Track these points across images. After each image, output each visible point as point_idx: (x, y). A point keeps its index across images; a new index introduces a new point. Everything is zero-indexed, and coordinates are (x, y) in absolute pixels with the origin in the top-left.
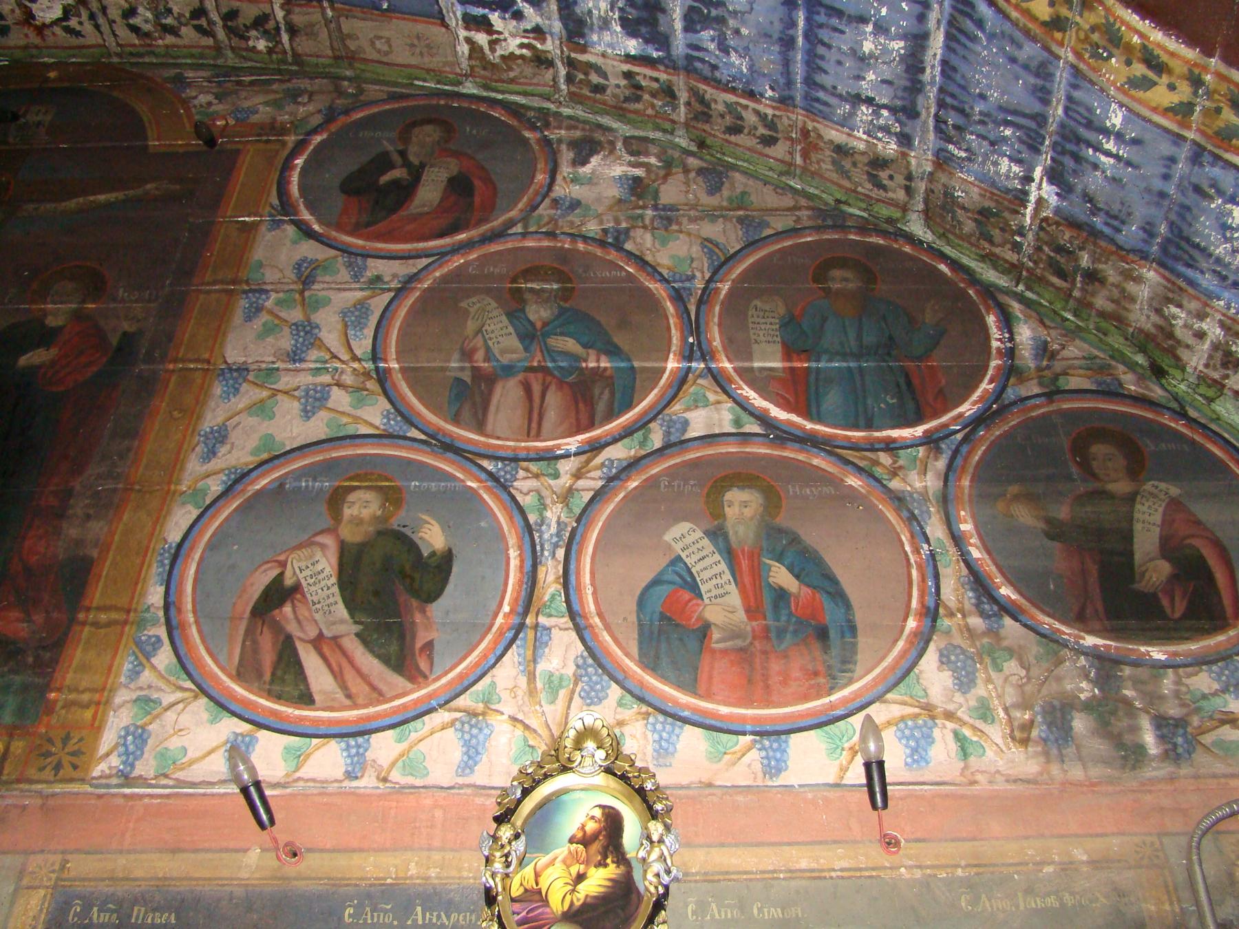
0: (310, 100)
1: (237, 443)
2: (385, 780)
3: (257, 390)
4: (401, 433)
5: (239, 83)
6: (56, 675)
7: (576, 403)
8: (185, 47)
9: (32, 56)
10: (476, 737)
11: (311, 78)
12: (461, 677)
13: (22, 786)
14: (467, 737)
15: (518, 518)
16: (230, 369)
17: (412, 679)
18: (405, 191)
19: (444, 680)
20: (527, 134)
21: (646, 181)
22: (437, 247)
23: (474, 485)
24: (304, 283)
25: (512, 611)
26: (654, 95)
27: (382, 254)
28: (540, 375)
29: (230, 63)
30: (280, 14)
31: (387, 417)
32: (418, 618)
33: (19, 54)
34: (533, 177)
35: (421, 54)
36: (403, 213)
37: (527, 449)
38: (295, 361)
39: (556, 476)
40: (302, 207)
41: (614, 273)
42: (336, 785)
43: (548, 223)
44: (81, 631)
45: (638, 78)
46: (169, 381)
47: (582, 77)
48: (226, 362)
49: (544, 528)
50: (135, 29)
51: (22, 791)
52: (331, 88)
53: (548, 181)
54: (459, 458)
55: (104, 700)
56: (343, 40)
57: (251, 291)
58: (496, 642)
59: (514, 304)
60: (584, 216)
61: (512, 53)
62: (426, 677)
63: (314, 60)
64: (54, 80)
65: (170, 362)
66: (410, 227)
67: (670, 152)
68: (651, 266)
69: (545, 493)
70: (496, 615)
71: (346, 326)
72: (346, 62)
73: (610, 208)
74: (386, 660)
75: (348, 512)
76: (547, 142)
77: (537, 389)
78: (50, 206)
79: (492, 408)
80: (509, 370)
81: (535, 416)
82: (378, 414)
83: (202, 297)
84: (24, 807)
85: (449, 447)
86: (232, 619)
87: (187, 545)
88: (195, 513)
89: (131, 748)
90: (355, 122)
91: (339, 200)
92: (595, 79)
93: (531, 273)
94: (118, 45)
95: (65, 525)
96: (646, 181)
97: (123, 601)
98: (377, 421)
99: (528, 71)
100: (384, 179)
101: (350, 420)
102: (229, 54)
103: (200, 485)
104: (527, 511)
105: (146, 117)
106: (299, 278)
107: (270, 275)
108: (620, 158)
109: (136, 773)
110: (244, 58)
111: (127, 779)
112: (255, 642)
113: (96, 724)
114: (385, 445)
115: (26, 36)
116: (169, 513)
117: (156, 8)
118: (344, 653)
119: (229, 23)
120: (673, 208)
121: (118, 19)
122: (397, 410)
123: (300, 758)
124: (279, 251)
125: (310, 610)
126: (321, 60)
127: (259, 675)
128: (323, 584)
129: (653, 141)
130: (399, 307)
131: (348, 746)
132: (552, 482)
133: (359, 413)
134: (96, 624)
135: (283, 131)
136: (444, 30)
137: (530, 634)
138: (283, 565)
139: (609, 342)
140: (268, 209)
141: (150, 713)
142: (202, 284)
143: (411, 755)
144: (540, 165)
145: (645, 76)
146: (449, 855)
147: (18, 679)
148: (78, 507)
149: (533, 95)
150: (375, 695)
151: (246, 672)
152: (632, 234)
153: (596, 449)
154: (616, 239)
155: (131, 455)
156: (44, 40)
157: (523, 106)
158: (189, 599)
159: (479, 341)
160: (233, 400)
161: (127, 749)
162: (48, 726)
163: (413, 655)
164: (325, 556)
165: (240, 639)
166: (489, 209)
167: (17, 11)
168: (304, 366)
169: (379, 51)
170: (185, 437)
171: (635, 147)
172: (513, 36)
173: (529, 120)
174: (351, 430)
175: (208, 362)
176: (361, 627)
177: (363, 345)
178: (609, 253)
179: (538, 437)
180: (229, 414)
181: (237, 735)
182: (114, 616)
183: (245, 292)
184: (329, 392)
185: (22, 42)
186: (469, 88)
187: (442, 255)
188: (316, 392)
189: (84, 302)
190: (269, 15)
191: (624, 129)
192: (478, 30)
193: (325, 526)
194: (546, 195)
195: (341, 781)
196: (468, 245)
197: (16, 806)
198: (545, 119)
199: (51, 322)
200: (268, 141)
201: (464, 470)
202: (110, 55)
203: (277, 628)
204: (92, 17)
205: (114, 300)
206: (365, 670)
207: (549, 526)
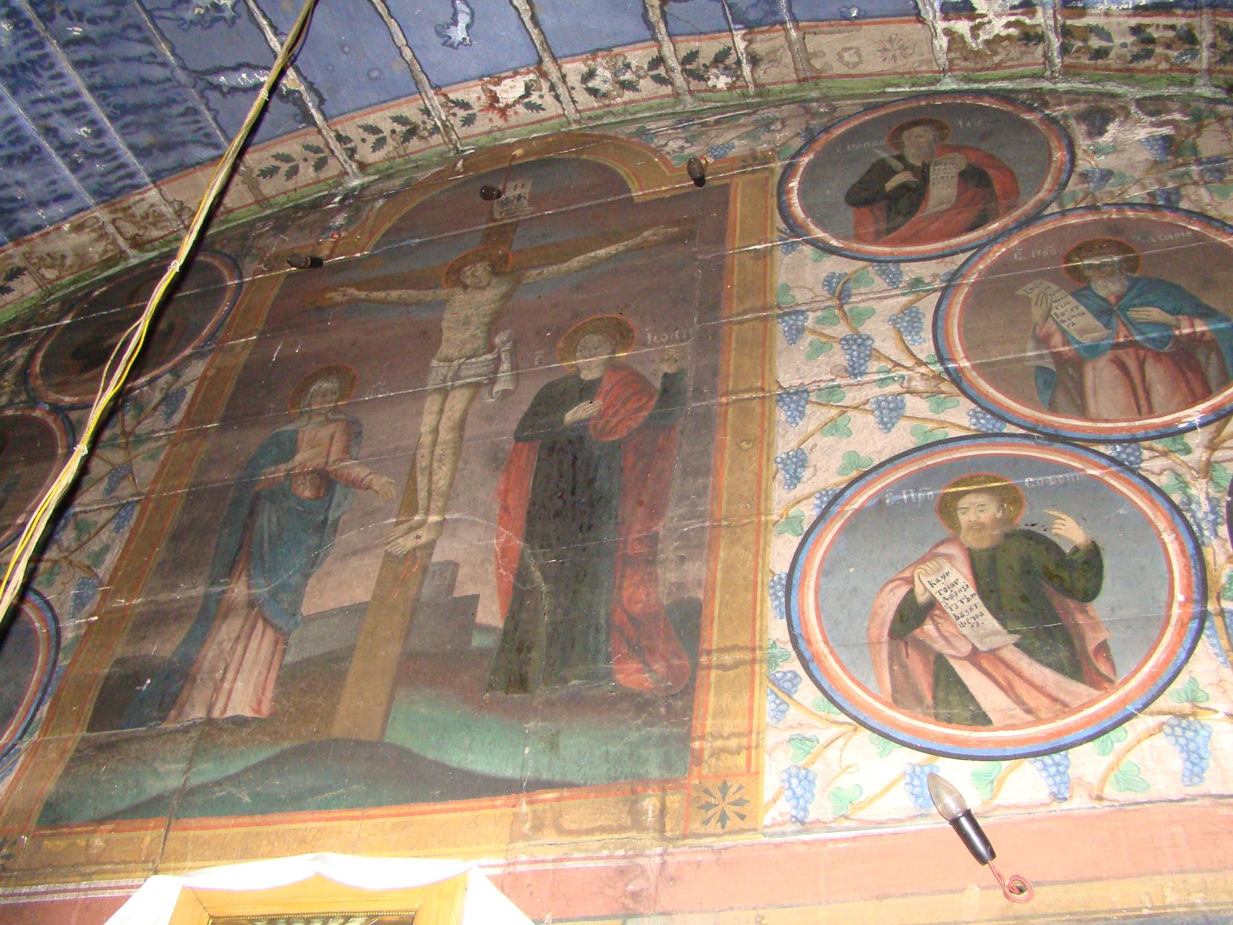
0: (784, 126)
1: (819, 465)
2: (1100, 798)
3: (824, 410)
4: (996, 431)
5: (704, 124)
6: (694, 722)
7: (1184, 374)
8: (644, 100)
9: (496, 140)
10: (1193, 740)
11: (776, 106)
12: (1152, 677)
13: (689, 841)
14: (1182, 741)
15: (1159, 500)
16: (788, 394)
17: (1095, 685)
18: (915, 193)
19: (1133, 683)
20: (1027, 117)
21: (1178, 139)
22: (970, 241)
23: (1096, 472)
24: (839, 298)
25: (1187, 600)
26: (1168, 46)
27: (914, 256)
28: (1131, 351)
29: (689, 107)
30: (741, 45)
31: (975, 415)
32: (1081, 619)
33: (484, 140)
34: (1050, 155)
35: (894, 58)
36: (920, 215)
37: (1145, 427)
38: (855, 376)
39: (1188, 451)
40: (812, 226)
41: (1177, 235)
42: (1043, 809)
43: (1084, 198)
44: (708, 676)
45: (1148, 30)
46: (726, 412)
47: (1080, 44)
48: (781, 387)
49: (1193, 506)
50: (594, 92)
51: (690, 847)
52: (803, 111)
53: (1068, 157)
54: (1068, 447)
55: (754, 744)
56: (808, 60)
57: (785, 314)
58: (1180, 635)
59: (1078, 284)
60: (1122, 184)
61: (998, 35)
62: (1111, 682)
63: (780, 87)
64: (520, 157)
65: (722, 396)
66: (933, 227)
67: (1194, 104)
68: (1217, 220)
69: (1182, 470)
70: (1169, 606)
71: (899, 332)
72: (811, 83)
73: (1148, 172)
74: (1059, 669)
75: (964, 519)
76: (1052, 121)
77: (1132, 364)
78: (553, 269)
79: (1089, 391)
80: (1094, 351)
81: (1141, 393)
82: (964, 415)
83: (735, 328)
84: (698, 863)
85: (1054, 438)
86: (870, 644)
87: (797, 574)
88: (796, 541)
89: (799, 791)
90: (839, 138)
91: (850, 213)
92: (1095, 43)
93: (1085, 249)
94: (578, 111)
95: (659, 571)
96: (1178, 139)
97: (744, 639)
98: (966, 422)
99: (1015, 51)
100: (891, 184)
101: (935, 425)
102: (688, 98)
103: (793, 512)
104: (1167, 491)
105: (622, 171)
106: (833, 294)
107: (801, 296)
108: (1139, 121)
109: (811, 817)
110: (703, 100)
111: (804, 825)
112: (903, 666)
113: (753, 770)
114: (982, 445)
115: (491, 120)
116: (767, 543)
117: (614, 66)
118: (1008, 666)
119: (688, 67)
120: (1218, 159)
121: (578, 85)
122: (983, 408)
123: (997, 784)
124: (803, 273)
125: (955, 625)
126: (787, 86)
127: (919, 700)
128: (961, 595)
129: (1170, 98)
130: (950, 305)
131: (1045, 765)
132: (1185, 458)
133: (942, 417)
134: (722, 667)
135: (766, 160)
136: (920, 26)
137: (1218, 621)
138: (910, 581)
139: (1199, 305)
140: (776, 234)
141: (809, 753)
142: (731, 316)
143: (1122, 767)
144: (1054, 144)
145: (1158, 26)
146: (1209, 877)
147: (656, 731)
148: (669, 550)
149: (1022, 77)
150: (1058, 707)
151: (903, 695)
152: (1183, 192)
153: (1223, 416)
154: (1168, 199)
155: (709, 492)
156: (506, 120)
157: (1011, 91)
158: (817, 630)
159: (1051, 326)
160: (801, 423)
161: (794, 793)
162: (699, 776)
163: (1088, 658)
164: (954, 566)
165: (886, 664)
166: (1012, 196)
167: (483, 97)
168: (866, 378)
169: (847, 65)
170: (760, 466)
171: (1154, 107)
172: (998, 15)
173: (1023, 102)
174: (940, 435)
175: (763, 390)
176: (1018, 636)
177: (925, 349)
178: (1165, 216)
179: (1151, 413)
180: (801, 438)
181: (913, 766)
182: (739, 655)
183: (779, 316)
184: (902, 401)
185: (487, 128)
186: (948, 84)
187: (979, 248)
188: (889, 403)
189: (614, 352)
190: (729, 49)
191: (1137, 93)
192: (958, 18)
193: (944, 537)
194: (1071, 171)
195: (1048, 805)
196: (1005, 234)
197: (688, 863)
198: (1040, 99)
199: (587, 376)
200: (753, 172)
201: (1080, 459)
202: (569, 123)
203: (923, 648)
204: (552, 88)
205: (645, 345)
206: (1037, 680)
207: (1199, 504)
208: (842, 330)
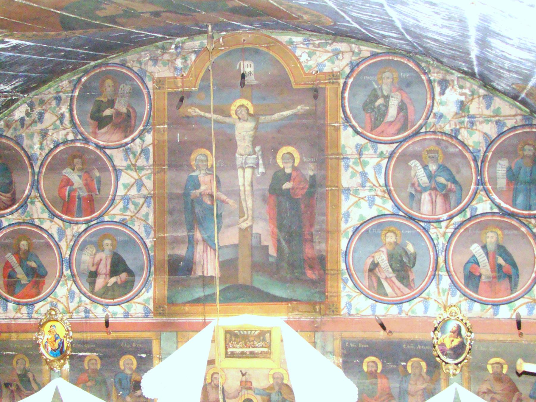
177: (382, 181)
208: (359, 169)
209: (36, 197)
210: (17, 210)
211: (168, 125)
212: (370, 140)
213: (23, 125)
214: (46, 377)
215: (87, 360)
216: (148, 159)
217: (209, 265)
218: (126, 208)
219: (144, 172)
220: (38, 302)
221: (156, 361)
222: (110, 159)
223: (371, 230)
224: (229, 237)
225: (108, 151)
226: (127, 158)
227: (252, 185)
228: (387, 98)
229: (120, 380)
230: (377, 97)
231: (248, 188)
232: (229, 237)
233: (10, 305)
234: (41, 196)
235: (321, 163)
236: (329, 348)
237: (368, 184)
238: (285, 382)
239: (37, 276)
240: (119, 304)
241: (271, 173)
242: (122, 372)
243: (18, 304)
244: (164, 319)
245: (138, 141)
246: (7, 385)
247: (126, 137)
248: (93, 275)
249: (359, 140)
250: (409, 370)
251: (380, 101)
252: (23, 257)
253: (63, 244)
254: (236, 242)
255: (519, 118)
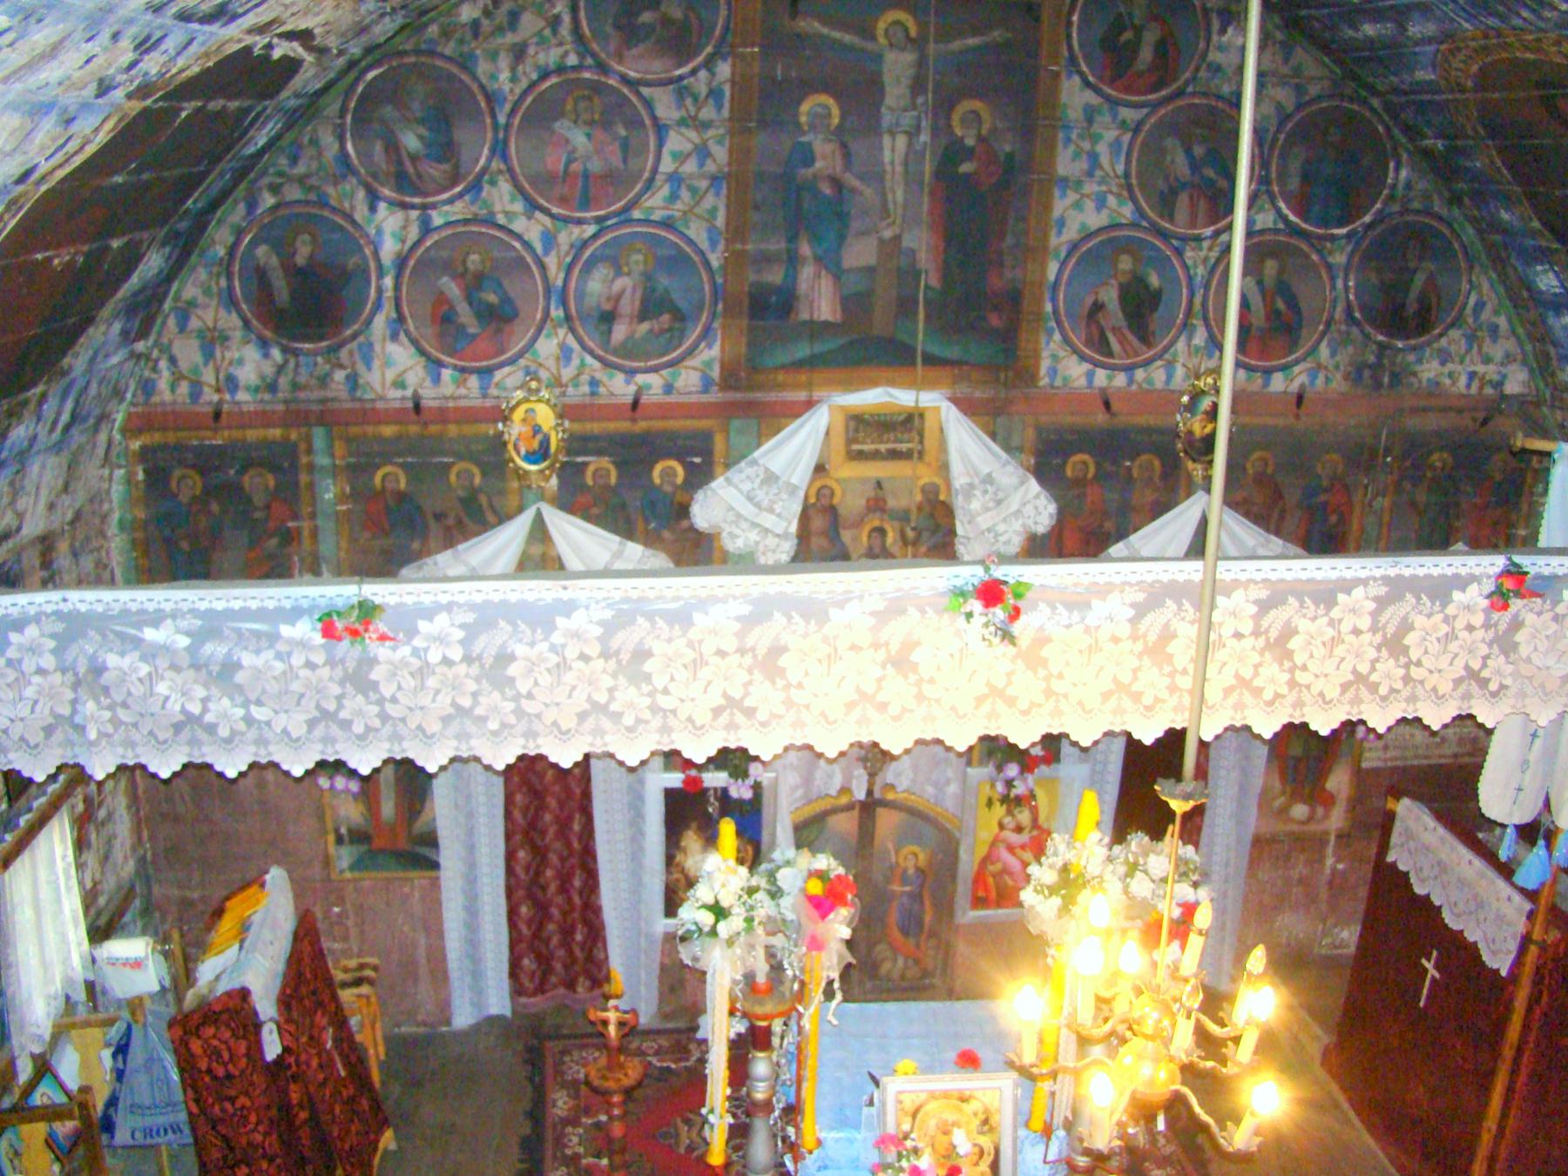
151: (1088, 343)
177: (1120, 169)
208: (1086, 145)
209: (500, 172)
210: (460, 196)
211: (762, 46)
212: (1108, 98)
213: (476, 35)
214: (513, 501)
215: (591, 469)
216: (719, 107)
217: (821, 300)
218: (674, 197)
219: (711, 133)
220: (501, 365)
221: (718, 469)
222: (648, 104)
223: (1098, 251)
224: (860, 253)
225: (645, 91)
226: (680, 104)
227: (906, 163)
228: (1138, 31)
229: (653, 504)
230: (1122, 29)
231: (899, 169)
232: (860, 253)
233: (447, 374)
234: (511, 170)
235: (1027, 134)
236: (1016, 441)
237: (1098, 173)
238: (942, 497)
239: (499, 317)
240: (655, 369)
241: (943, 142)
242: (659, 488)
243: (463, 370)
244: (738, 396)
245: (703, 74)
246: (439, 517)
247: (680, 66)
248: (608, 318)
249: (1090, 97)
250: (1135, 473)
251: (1128, 35)
252: (474, 284)
253: (551, 261)
254: (872, 261)
255: (1327, 83)
